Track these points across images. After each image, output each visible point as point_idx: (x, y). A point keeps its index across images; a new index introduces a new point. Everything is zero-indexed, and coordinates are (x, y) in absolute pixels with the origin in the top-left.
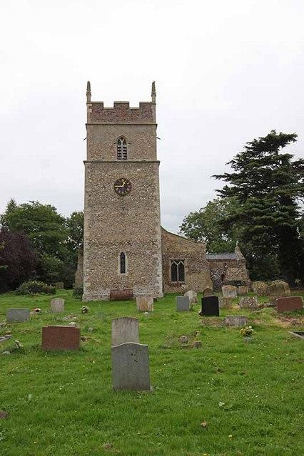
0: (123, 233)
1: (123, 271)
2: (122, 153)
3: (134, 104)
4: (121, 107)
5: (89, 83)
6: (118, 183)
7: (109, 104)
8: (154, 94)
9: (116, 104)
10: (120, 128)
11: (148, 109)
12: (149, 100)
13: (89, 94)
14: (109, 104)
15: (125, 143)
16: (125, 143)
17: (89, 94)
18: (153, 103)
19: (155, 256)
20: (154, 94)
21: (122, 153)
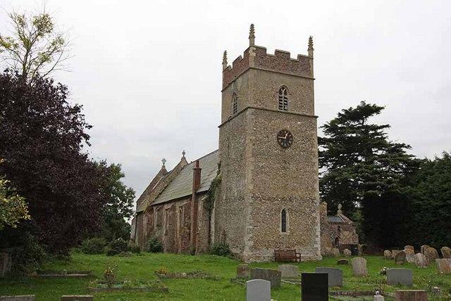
0: (285, 187)
1: (284, 230)
2: (283, 103)
3: (294, 56)
4: (282, 55)
5: (252, 26)
6: (282, 133)
7: (271, 52)
8: (311, 48)
9: (277, 52)
10: (281, 77)
11: (305, 63)
12: (307, 54)
13: (252, 37)
14: (271, 52)
15: (285, 93)
16: (285, 93)
17: (252, 37)
18: (310, 58)
19: (314, 215)
20: (311, 48)
21: (283, 103)
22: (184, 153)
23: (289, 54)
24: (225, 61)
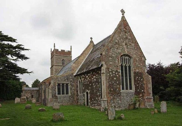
4: (63, 51)
7: (60, 50)
8: (71, 49)
12: (70, 50)
13: (54, 46)
14: (60, 50)
17: (54, 46)
20: (71, 49)
22: (91, 38)
23: (58, 50)
24: (51, 51)
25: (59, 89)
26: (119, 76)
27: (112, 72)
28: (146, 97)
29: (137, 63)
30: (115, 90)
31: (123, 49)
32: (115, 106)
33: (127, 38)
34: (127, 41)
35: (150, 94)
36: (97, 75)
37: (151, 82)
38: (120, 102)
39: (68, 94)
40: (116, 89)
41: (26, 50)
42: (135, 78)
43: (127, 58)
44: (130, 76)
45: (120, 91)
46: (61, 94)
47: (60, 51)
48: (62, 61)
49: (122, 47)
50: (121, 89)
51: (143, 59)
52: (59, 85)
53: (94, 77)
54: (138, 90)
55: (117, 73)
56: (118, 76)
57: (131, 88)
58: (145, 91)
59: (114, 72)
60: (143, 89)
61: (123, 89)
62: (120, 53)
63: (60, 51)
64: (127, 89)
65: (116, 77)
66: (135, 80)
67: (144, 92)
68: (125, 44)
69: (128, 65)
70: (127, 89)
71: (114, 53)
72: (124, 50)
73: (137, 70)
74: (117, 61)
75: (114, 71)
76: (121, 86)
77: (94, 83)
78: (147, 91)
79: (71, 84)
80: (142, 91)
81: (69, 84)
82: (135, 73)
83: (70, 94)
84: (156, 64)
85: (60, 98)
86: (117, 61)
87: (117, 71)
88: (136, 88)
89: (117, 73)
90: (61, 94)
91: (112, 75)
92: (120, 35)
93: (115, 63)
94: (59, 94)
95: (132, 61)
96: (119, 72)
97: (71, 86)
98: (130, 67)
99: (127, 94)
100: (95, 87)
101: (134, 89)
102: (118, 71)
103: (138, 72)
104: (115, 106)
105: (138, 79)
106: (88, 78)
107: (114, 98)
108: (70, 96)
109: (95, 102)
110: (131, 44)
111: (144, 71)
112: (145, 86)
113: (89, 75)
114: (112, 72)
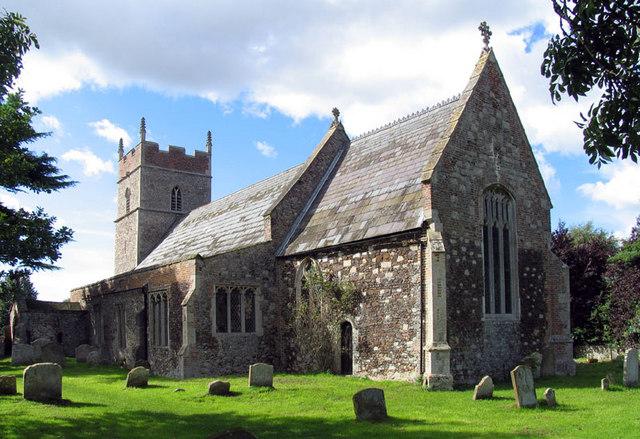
4: (177, 153)
7: (164, 148)
8: (210, 144)
13: (143, 131)
14: (164, 148)
17: (143, 131)
20: (210, 144)
25: (221, 309)
26: (479, 261)
27: (458, 248)
28: (550, 340)
29: (528, 220)
30: (465, 315)
31: (489, 168)
32: (465, 371)
33: (499, 126)
34: (500, 137)
35: (562, 326)
36: (400, 259)
37: (568, 286)
38: (479, 355)
39: (254, 330)
40: (469, 312)
41: (39, 135)
42: (521, 271)
43: (500, 197)
44: (507, 265)
45: (479, 319)
46: (229, 331)
47: (167, 149)
48: (174, 193)
49: (485, 157)
50: (484, 311)
51: (543, 202)
52: (221, 293)
53: (386, 265)
54: (530, 314)
55: (472, 254)
56: (474, 262)
57: (508, 310)
58: (549, 317)
59: (464, 249)
60: (542, 312)
61: (488, 311)
62: (480, 181)
63: (167, 149)
64: (498, 311)
65: (469, 266)
66: (522, 279)
67: (544, 322)
68: (495, 149)
69: (500, 226)
70: (498, 311)
71: (462, 178)
72: (493, 170)
73: (528, 245)
74: (472, 210)
75: (464, 244)
76: (484, 299)
77: (382, 286)
78: (553, 314)
79: (266, 294)
80: (541, 316)
81: (258, 292)
82: (522, 253)
83: (259, 330)
84: (17, 210)
85: (226, 346)
86: (472, 210)
87: (471, 246)
88: (525, 305)
89: (472, 254)
90: (229, 331)
91: (458, 261)
92: (481, 115)
93: (467, 215)
94: (222, 328)
95: (513, 205)
96: (478, 250)
97: (266, 298)
98: (506, 232)
99: (501, 327)
100: (387, 301)
101: (520, 311)
102: (477, 244)
103: (529, 251)
104: (465, 371)
105: (530, 273)
106: (354, 270)
107: (463, 343)
108: (260, 339)
109: (387, 359)
110: (509, 150)
111: (546, 246)
112: (548, 300)
113: (357, 255)
114: (458, 248)
